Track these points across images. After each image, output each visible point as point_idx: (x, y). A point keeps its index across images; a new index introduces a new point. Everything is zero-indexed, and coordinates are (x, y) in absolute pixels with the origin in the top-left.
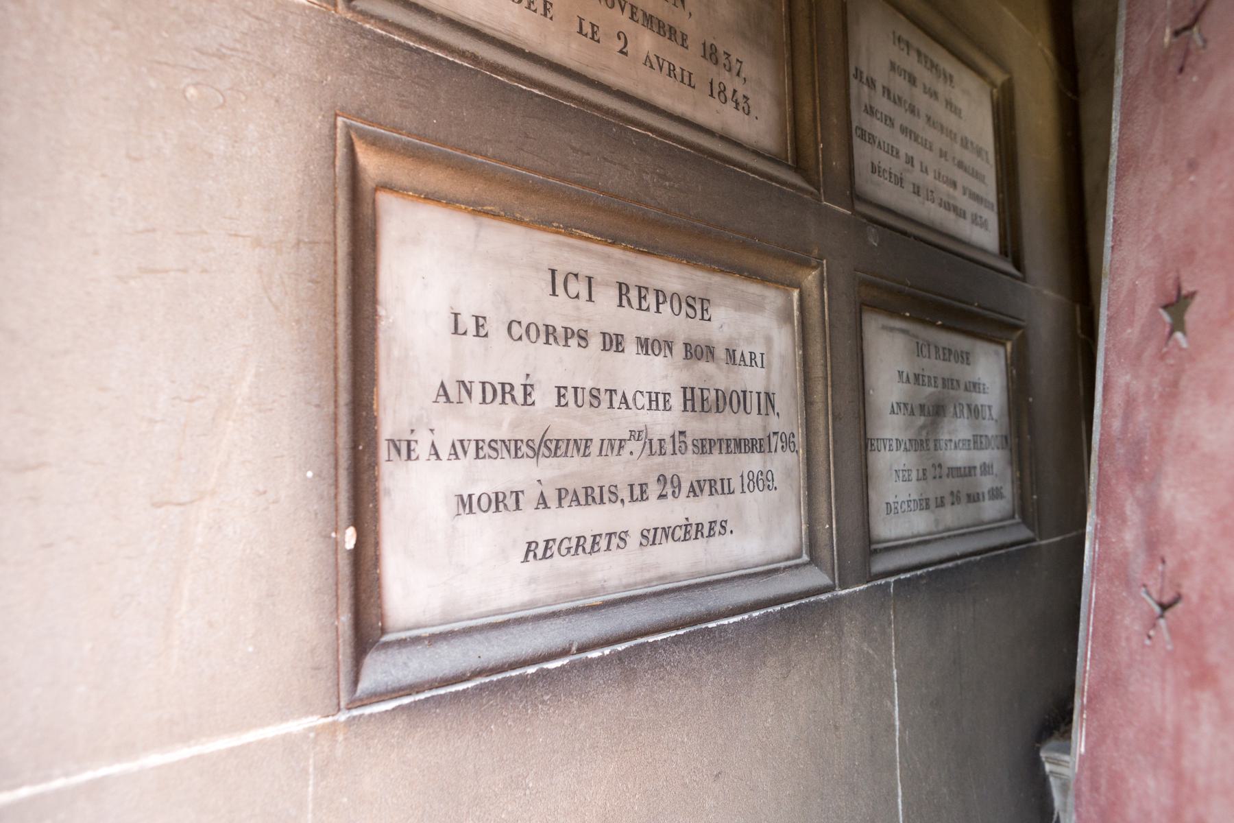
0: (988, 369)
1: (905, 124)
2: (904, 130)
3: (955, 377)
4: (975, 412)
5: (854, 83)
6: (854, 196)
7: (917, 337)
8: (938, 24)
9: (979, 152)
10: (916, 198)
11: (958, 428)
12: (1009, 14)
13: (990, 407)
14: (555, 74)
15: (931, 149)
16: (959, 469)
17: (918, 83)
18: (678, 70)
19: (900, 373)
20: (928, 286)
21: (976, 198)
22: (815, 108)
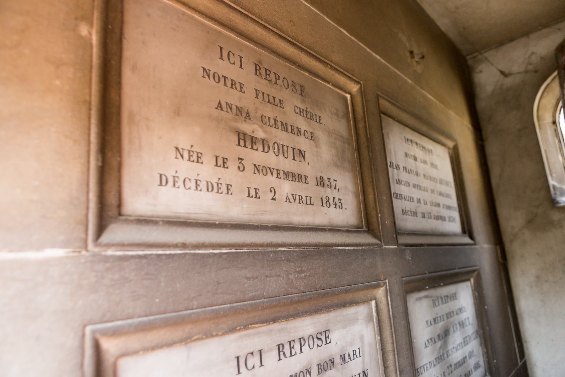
0: (464, 296)
1: (415, 183)
2: (415, 186)
3: (451, 311)
4: (462, 325)
5: (390, 169)
6: (397, 232)
7: (431, 297)
8: (424, 129)
9: (447, 184)
10: (423, 220)
11: (456, 338)
12: (452, 113)
13: (468, 318)
14: (235, 231)
15: (427, 191)
16: (459, 362)
17: (418, 159)
18: (304, 198)
19: (427, 322)
20: (432, 266)
21: (449, 208)
22: (374, 195)
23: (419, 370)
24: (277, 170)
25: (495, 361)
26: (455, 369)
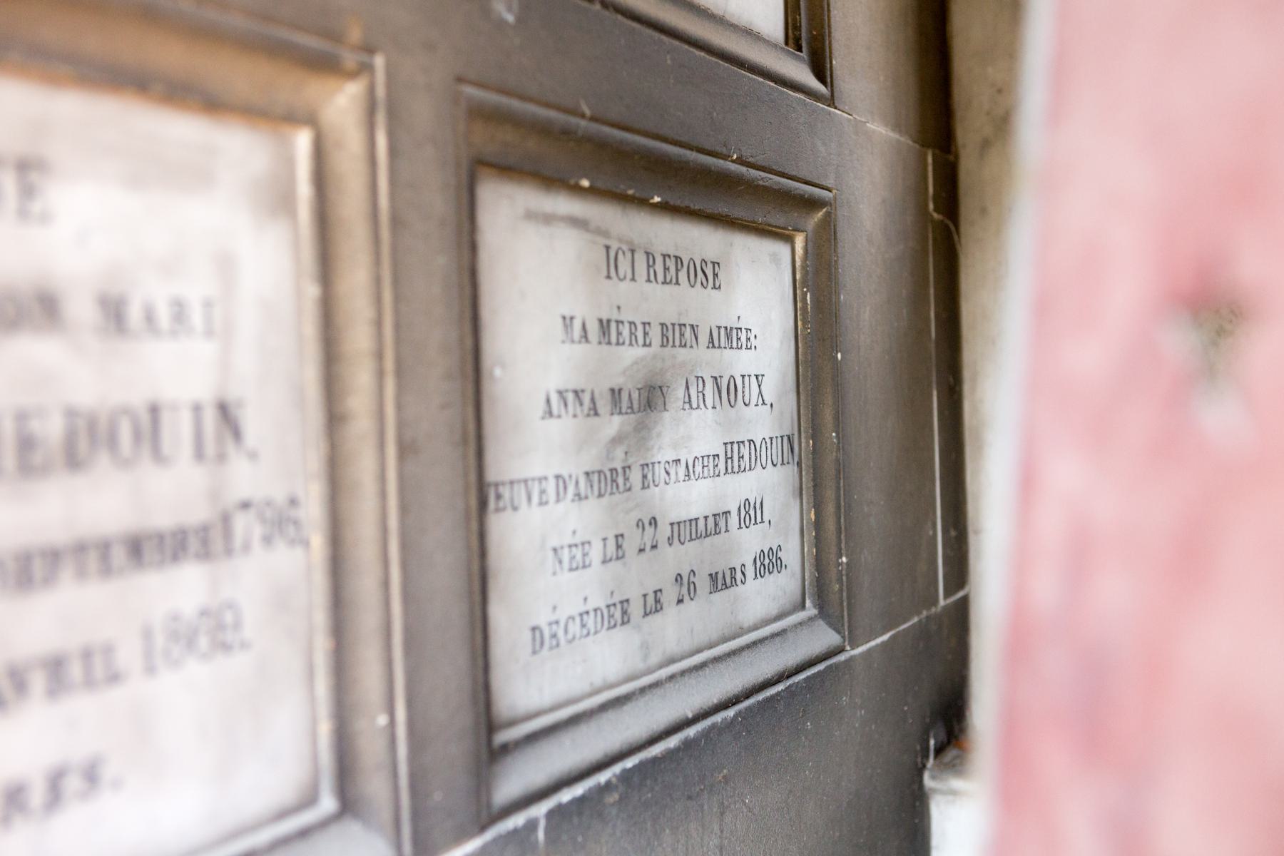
0: (755, 287)
11: (692, 431)
19: (567, 321)
23: (505, 491)
24: (757, 376)
25: (844, 559)
26: (670, 541)
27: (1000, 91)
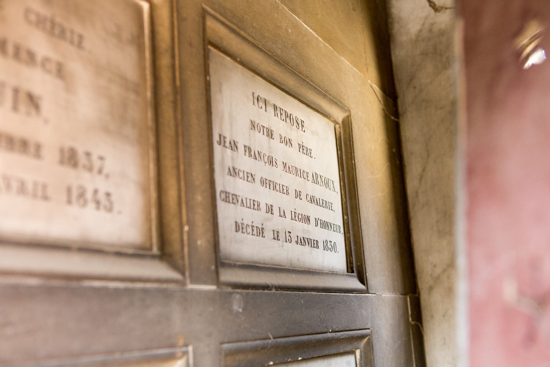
27: (435, 266)
